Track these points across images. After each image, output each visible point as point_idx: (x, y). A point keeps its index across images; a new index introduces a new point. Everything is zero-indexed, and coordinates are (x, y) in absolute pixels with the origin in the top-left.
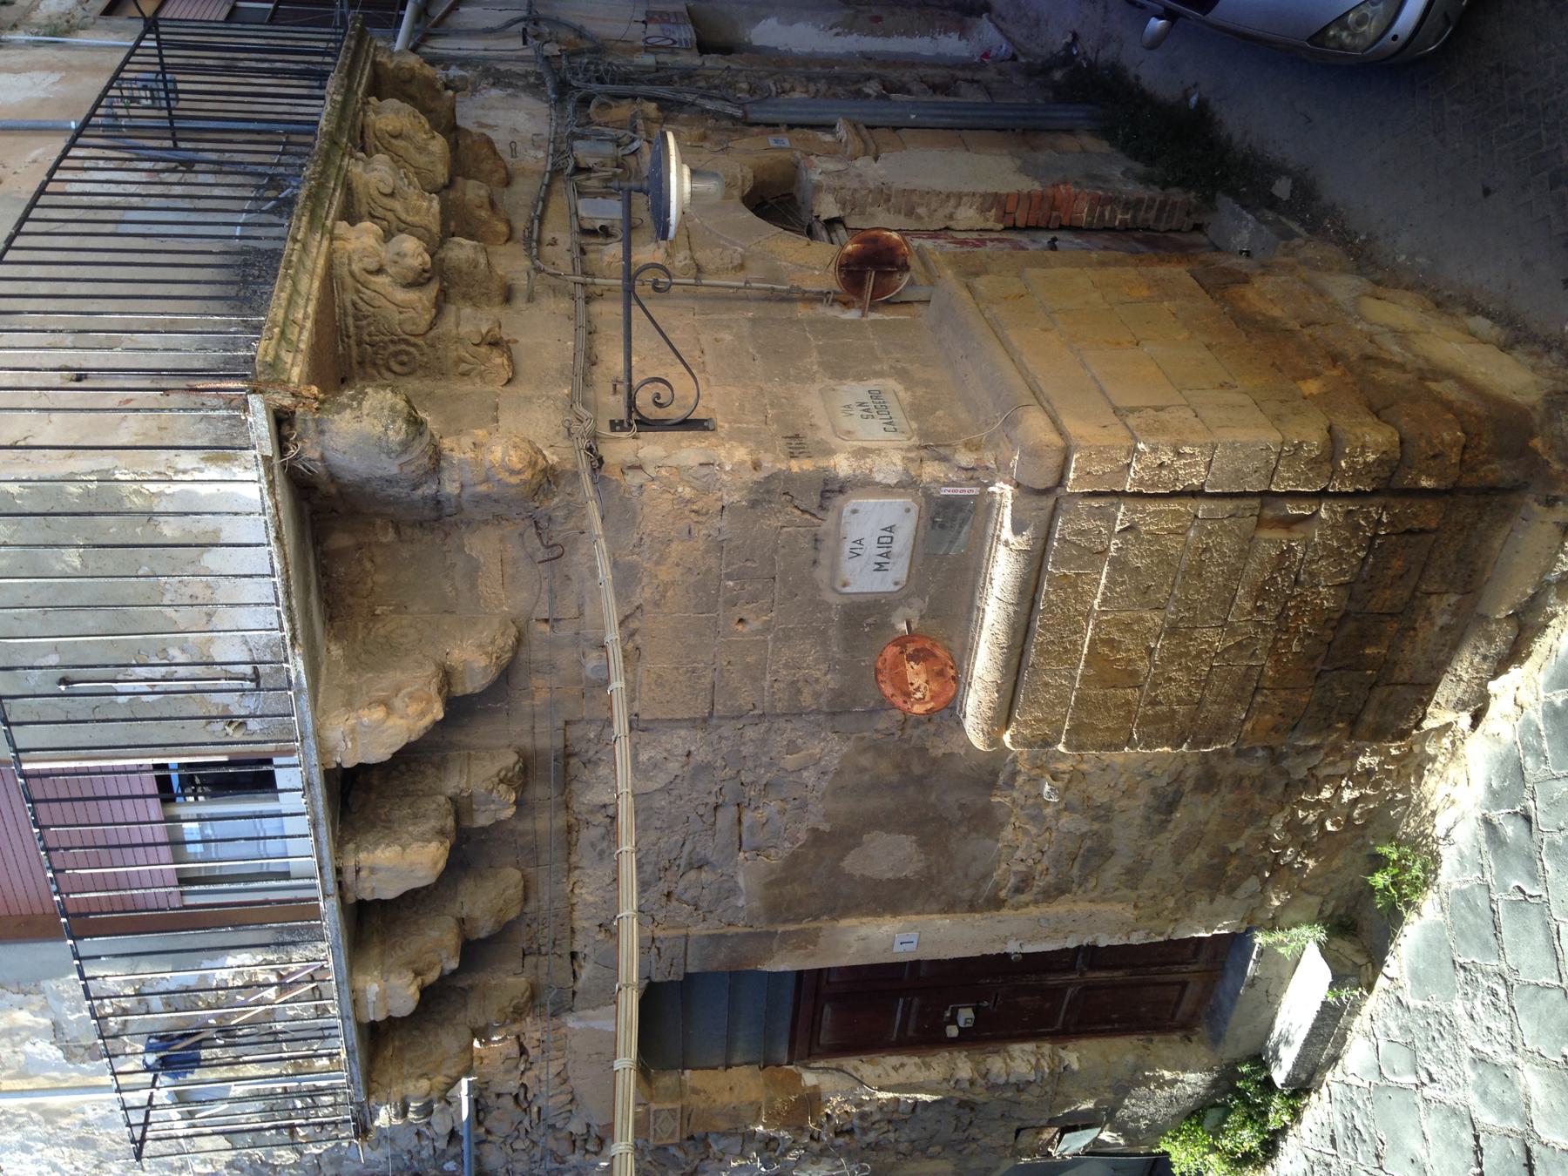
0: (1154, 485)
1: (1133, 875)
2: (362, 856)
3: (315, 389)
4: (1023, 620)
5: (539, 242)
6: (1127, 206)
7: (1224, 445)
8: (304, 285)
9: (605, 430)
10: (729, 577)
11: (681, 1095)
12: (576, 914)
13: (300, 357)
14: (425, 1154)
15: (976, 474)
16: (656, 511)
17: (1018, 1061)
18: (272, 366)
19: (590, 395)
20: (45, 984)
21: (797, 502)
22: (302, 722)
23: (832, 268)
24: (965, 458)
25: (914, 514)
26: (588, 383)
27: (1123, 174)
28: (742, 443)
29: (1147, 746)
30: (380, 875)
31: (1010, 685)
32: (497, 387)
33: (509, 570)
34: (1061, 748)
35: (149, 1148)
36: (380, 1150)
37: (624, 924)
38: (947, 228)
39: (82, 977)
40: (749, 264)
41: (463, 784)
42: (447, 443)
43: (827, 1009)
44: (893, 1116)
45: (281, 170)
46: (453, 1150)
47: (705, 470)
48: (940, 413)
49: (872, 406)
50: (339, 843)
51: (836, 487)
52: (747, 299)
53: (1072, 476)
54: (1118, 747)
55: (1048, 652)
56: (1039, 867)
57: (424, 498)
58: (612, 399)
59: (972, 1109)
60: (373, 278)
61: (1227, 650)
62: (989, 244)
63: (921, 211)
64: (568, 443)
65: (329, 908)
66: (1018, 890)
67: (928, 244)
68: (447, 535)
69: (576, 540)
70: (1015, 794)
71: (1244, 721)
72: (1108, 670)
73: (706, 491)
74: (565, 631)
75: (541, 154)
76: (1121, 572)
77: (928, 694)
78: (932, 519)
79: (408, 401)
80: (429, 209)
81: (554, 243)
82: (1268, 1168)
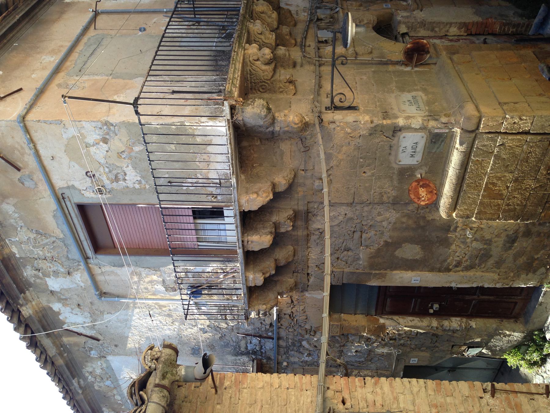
0: (511, 130)
1: (499, 264)
2: (249, 237)
3: (241, 99)
4: (462, 175)
5: (305, 46)
6: (514, 26)
7: (538, 116)
8: (237, 67)
9: (323, 110)
10: (361, 158)
11: (340, 321)
12: (309, 262)
13: (237, 89)
14: (263, 329)
15: (448, 125)
16: (339, 136)
17: (454, 323)
18: (230, 92)
19: (319, 98)
20: (161, 268)
21: (385, 134)
22: (234, 197)
23: (402, 52)
24: (444, 120)
25: (425, 139)
26: (319, 95)
27: (514, 14)
28: (367, 114)
29: (505, 220)
30: (254, 243)
31: (456, 197)
32: (291, 96)
33: (293, 154)
34: (473, 219)
35: (188, 317)
36: (250, 327)
37: (325, 262)
38: (446, 35)
39: (174, 266)
40: (374, 51)
41: (277, 219)
42: (277, 115)
43: (389, 300)
44: (409, 335)
45: (226, 24)
46: (271, 329)
47: (355, 123)
48: (437, 104)
49: (413, 101)
50: (243, 234)
51: (398, 129)
52: (372, 64)
53: (481, 126)
54: (495, 220)
55: (470, 186)
56: (464, 259)
57: (269, 132)
58: (326, 100)
59: (437, 337)
60: (256, 62)
61: (536, 188)
62: (461, 41)
63: (437, 29)
64: (312, 114)
65: (240, 251)
66: (456, 266)
67: (437, 41)
68: (275, 143)
69: (313, 145)
70: (457, 234)
71: (541, 213)
72: (492, 193)
73: (355, 130)
74: (309, 174)
75: (306, 14)
76: (498, 160)
77: (426, 199)
78: (431, 140)
79: (267, 103)
80: (271, 38)
81: (309, 46)
82: (543, 367)
